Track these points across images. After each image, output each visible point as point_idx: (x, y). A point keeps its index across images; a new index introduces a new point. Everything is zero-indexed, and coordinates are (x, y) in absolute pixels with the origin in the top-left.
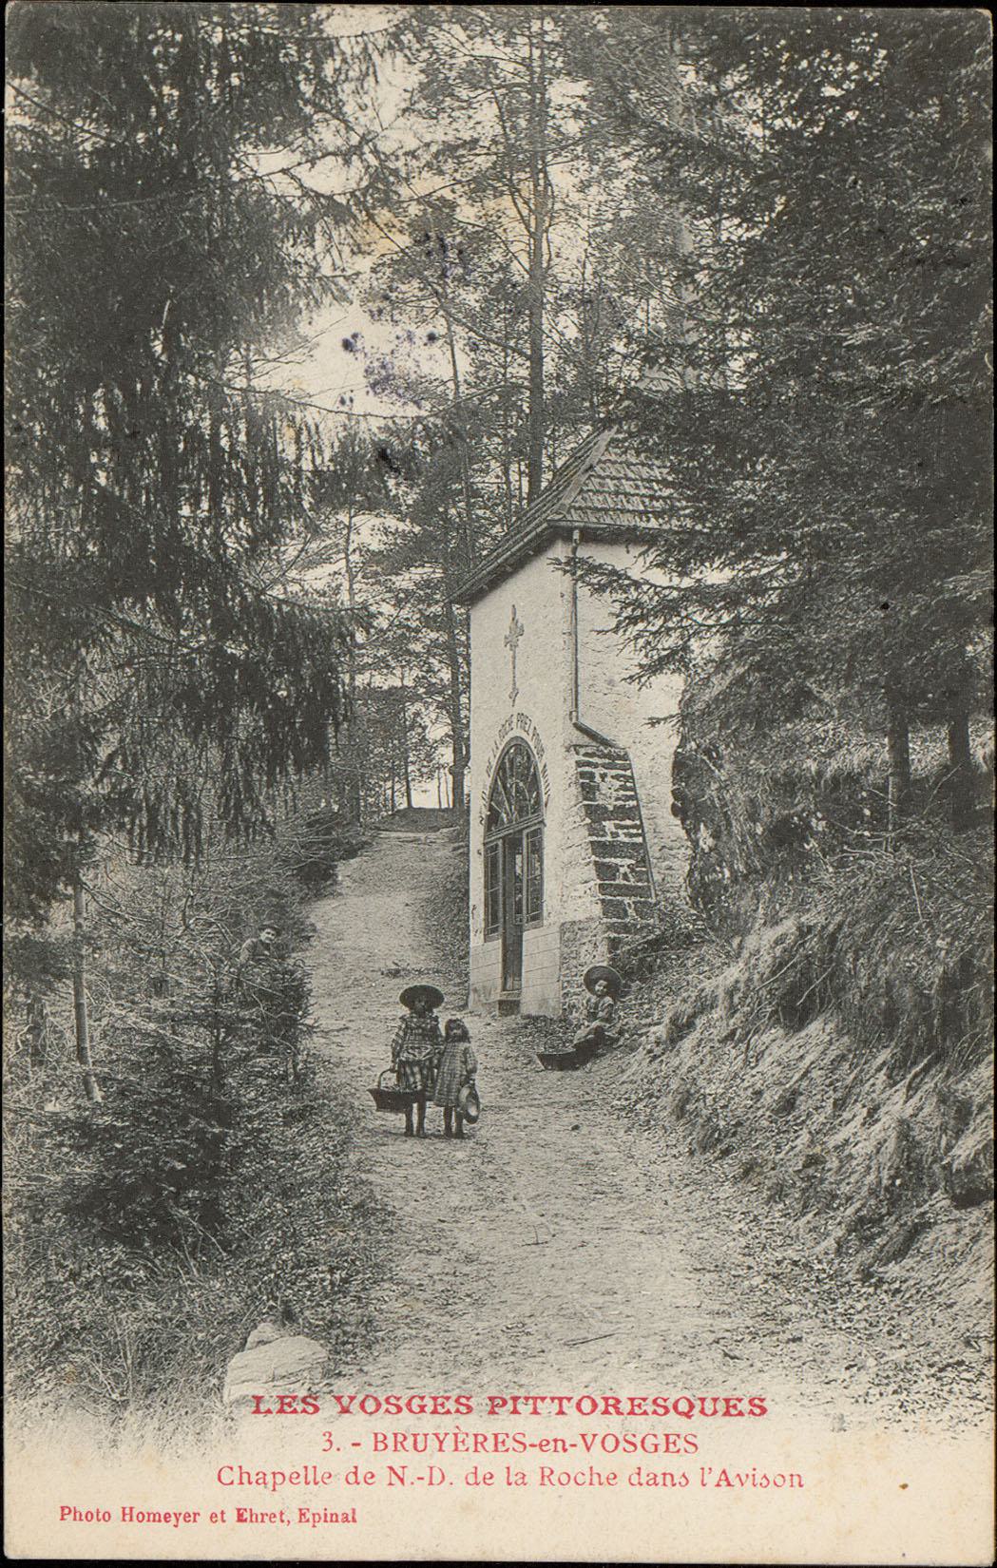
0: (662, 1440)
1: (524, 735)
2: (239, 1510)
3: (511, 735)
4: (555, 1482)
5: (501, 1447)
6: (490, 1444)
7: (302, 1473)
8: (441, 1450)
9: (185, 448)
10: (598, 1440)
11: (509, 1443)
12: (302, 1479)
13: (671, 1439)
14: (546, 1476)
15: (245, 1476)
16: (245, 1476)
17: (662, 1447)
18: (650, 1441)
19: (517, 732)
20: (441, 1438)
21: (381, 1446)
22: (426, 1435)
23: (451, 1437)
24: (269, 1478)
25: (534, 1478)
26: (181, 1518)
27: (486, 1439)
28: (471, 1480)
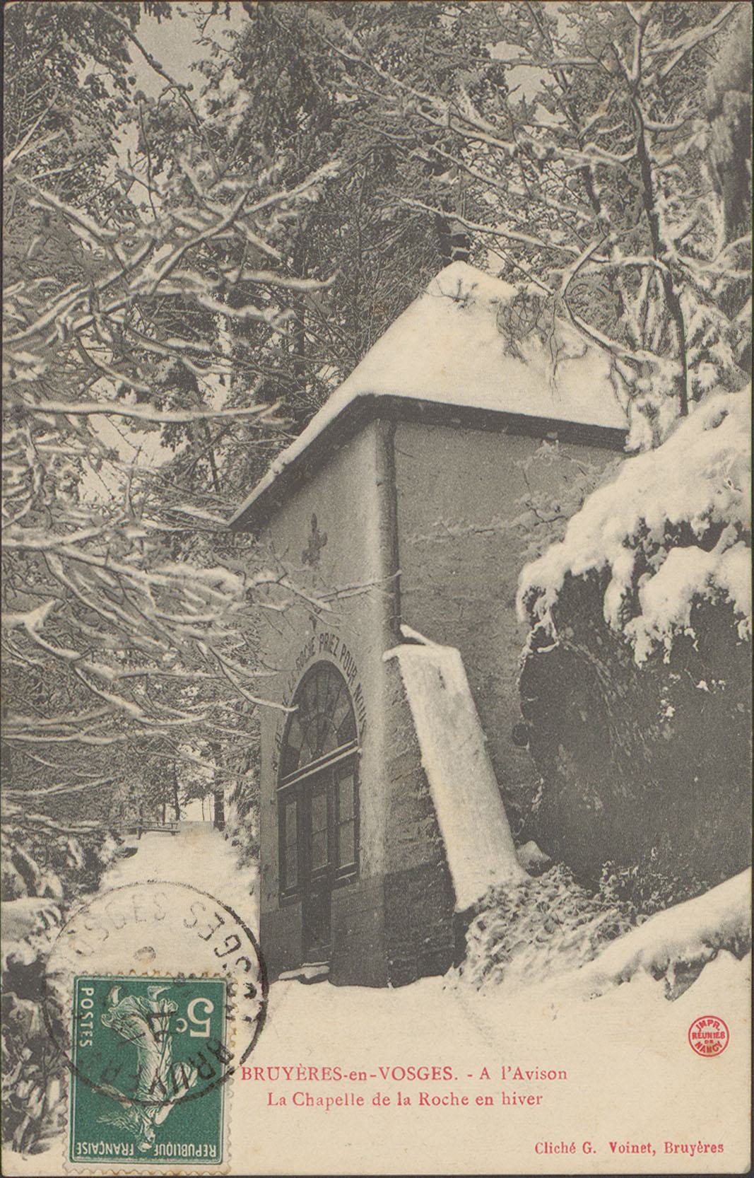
0: (431, 1071)
1: (331, 658)
2: (611, 1144)
3: (313, 660)
4: (430, 1102)
5: (326, 1076)
6: (319, 1075)
7: (344, 1098)
8: (288, 1079)
9: (742, 205)
10: (391, 1070)
11: (332, 1074)
12: (344, 1102)
13: (326, 1071)
14: (423, 1100)
15: (506, 1099)
16: (506, 1099)
17: (431, 1076)
18: (423, 1072)
19: (320, 656)
20: (288, 1070)
21: (247, 1076)
22: (278, 1068)
23: (295, 1070)
24: (325, 1101)
25: (415, 1101)
26: (696, 1150)
27: (316, 1070)
28: (376, 1102)
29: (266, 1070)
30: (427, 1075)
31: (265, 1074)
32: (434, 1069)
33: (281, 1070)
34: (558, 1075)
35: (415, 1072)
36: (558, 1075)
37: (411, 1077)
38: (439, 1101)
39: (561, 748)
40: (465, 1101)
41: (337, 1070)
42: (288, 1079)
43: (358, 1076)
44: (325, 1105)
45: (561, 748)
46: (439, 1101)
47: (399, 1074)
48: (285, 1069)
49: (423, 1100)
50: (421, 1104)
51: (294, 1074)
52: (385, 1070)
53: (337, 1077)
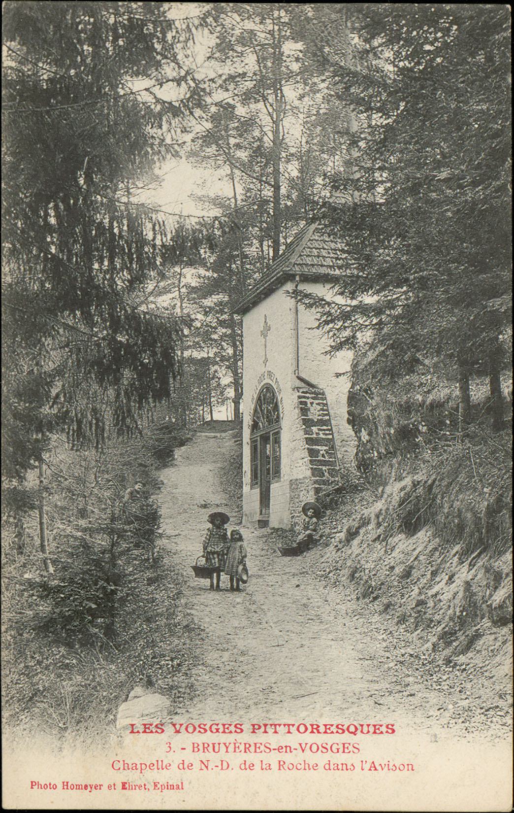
0: (341, 746)
4: (286, 768)
6: (252, 749)
7: (155, 763)
8: (227, 752)
10: (308, 746)
14: (281, 765)
15: (126, 765)
17: (341, 750)
20: (227, 745)
21: (196, 749)
23: (232, 746)
24: (139, 766)
28: (181, 766)
29: (211, 745)
30: (338, 749)
31: (211, 749)
32: (344, 744)
33: (222, 745)
34: (406, 766)
35: (207, 727)
36: (406, 766)
37: (325, 750)
38: (294, 767)
39: (363, 429)
40: (55, 787)
41: (267, 745)
42: (227, 752)
43: (284, 749)
44: (140, 769)
45: (363, 429)
46: (294, 767)
47: (314, 748)
48: (225, 744)
49: (281, 765)
50: (280, 769)
51: (231, 749)
52: (303, 746)
53: (268, 750)
